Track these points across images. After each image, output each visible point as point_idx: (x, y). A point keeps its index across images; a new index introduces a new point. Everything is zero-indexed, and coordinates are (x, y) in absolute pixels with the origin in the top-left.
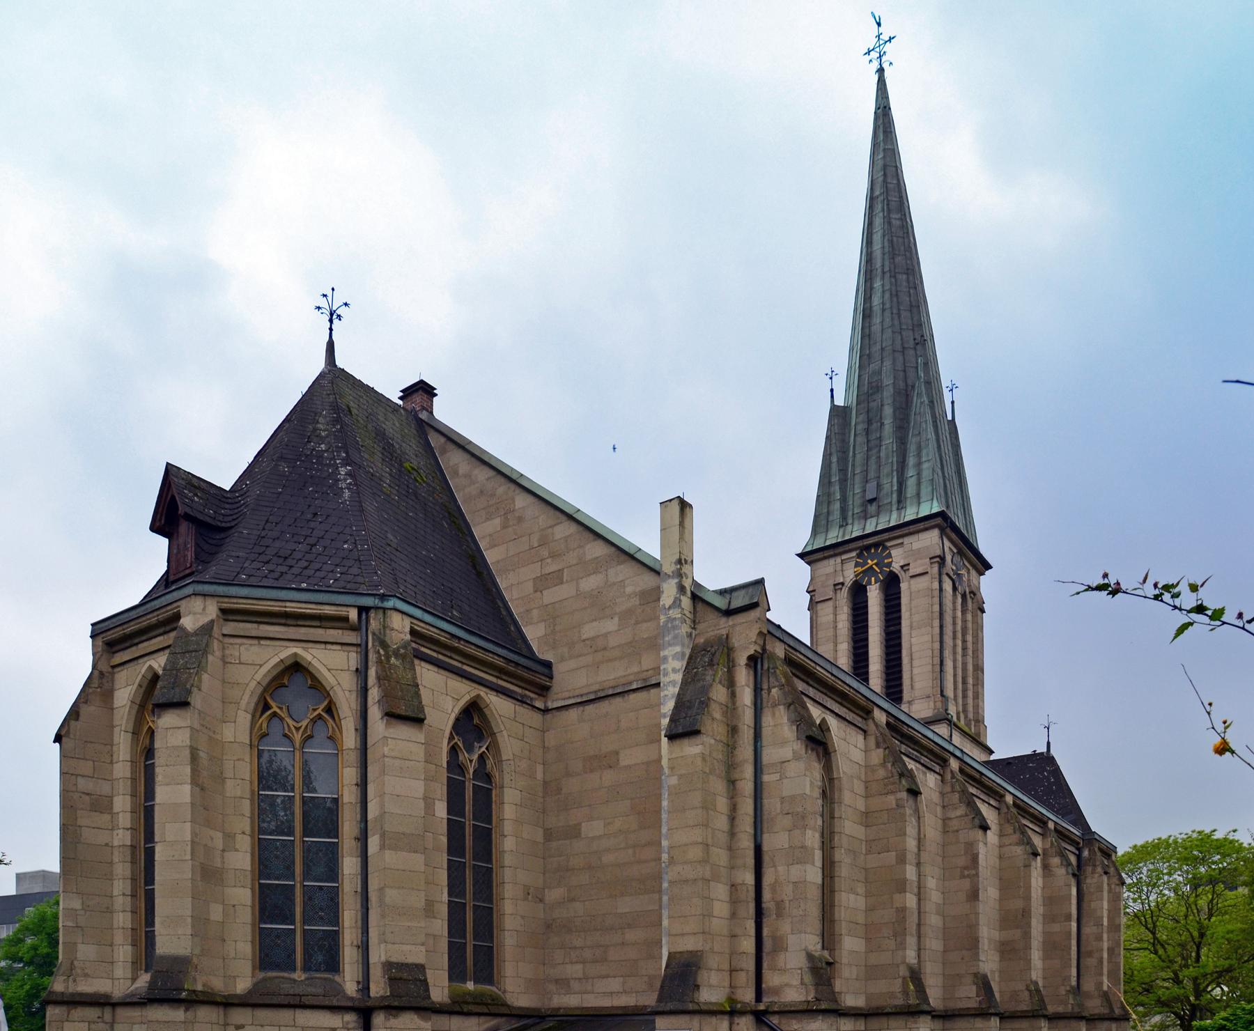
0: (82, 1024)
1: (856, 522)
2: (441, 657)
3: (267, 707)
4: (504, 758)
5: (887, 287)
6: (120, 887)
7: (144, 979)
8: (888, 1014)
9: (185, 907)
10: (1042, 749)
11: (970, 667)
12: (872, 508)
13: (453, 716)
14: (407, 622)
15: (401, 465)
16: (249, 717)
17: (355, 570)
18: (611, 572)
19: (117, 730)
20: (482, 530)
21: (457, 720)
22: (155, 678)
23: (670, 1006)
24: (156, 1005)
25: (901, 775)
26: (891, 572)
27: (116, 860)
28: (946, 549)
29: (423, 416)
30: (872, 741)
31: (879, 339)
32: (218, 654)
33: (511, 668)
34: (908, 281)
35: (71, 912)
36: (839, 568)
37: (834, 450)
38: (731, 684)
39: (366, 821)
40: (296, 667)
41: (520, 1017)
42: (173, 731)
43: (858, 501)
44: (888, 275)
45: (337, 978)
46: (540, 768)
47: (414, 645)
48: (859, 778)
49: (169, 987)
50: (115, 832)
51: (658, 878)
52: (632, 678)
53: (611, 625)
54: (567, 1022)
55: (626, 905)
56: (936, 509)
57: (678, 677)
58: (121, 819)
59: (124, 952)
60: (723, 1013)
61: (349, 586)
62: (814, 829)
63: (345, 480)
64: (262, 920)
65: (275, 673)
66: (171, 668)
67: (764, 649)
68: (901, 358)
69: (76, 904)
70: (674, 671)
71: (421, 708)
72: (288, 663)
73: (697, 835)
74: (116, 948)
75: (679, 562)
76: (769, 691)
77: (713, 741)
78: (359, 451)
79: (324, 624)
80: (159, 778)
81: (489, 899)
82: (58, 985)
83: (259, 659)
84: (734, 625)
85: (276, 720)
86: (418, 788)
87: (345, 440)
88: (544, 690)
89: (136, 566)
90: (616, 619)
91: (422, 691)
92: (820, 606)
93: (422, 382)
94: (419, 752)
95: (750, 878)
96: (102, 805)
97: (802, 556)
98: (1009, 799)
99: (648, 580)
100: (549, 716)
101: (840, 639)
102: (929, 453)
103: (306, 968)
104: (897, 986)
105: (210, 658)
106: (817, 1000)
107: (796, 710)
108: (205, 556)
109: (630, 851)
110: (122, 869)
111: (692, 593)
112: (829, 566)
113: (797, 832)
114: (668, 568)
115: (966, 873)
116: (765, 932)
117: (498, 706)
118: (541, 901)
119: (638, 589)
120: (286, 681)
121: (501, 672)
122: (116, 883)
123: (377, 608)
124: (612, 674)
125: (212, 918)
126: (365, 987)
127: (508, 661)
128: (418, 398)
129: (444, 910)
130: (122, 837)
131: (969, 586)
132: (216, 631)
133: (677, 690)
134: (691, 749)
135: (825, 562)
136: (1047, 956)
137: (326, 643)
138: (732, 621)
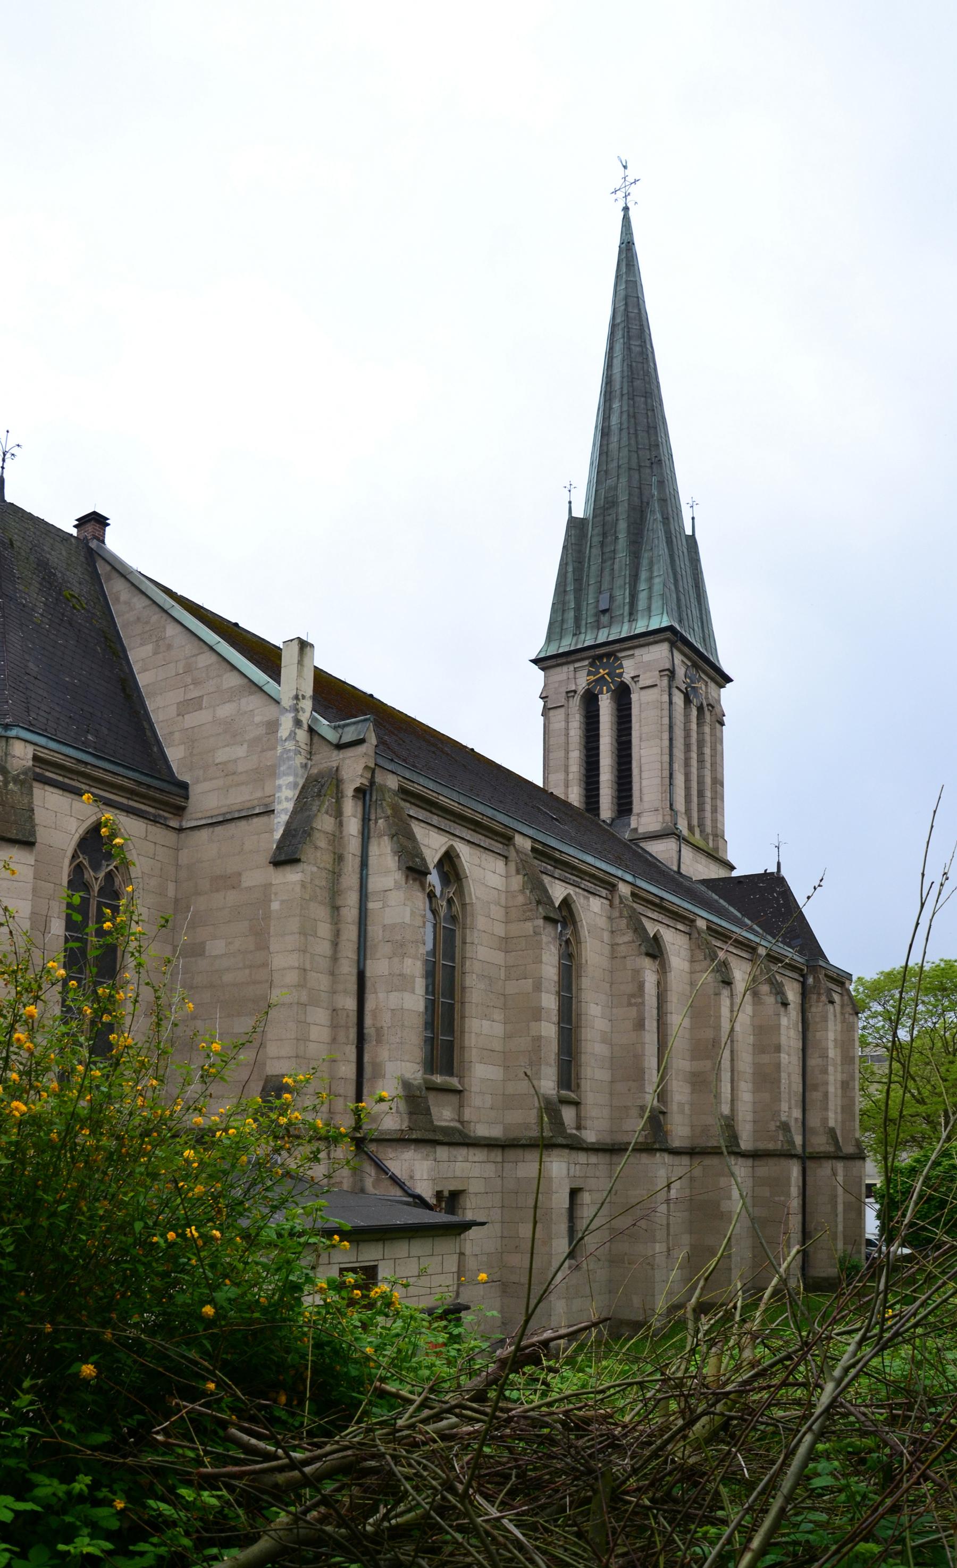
1: (589, 631)
5: (625, 409)
8: (524, 1146)
10: (772, 869)
11: (708, 780)
12: (605, 619)
13: (77, 837)
14: (30, 750)
15: (60, 593)
25: (539, 902)
26: (622, 682)
28: (676, 662)
29: (94, 544)
30: (512, 866)
31: (616, 457)
33: (143, 790)
34: (646, 403)
36: (572, 675)
37: (570, 560)
38: (338, 814)
43: (591, 610)
44: (625, 397)
46: (171, 887)
47: (38, 770)
48: (499, 904)
52: (256, 802)
53: (241, 751)
56: (664, 624)
57: (290, 806)
62: (415, 958)
67: (372, 782)
68: (637, 476)
70: (287, 799)
75: (296, 697)
76: (376, 822)
77: (315, 869)
84: (344, 759)
88: (179, 811)
90: (245, 746)
92: (552, 713)
93: (94, 513)
95: (351, 1003)
97: (535, 661)
98: (702, 924)
100: (183, 835)
101: (571, 747)
102: (661, 568)
104: (532, 1116)
106: (411, 1129)
107: (399, 842)
111: (309, 726)
112: (562, 674)
113: (396, 960)
115: (633, 1001)
116: (366, 1058)
119: (266, 719)
121: (131, 793)
127: (140, 783)
128: (90, 527)
131: (707, 698)
134: (292, 876)
135: (558, 669)
136: (757, 1089)
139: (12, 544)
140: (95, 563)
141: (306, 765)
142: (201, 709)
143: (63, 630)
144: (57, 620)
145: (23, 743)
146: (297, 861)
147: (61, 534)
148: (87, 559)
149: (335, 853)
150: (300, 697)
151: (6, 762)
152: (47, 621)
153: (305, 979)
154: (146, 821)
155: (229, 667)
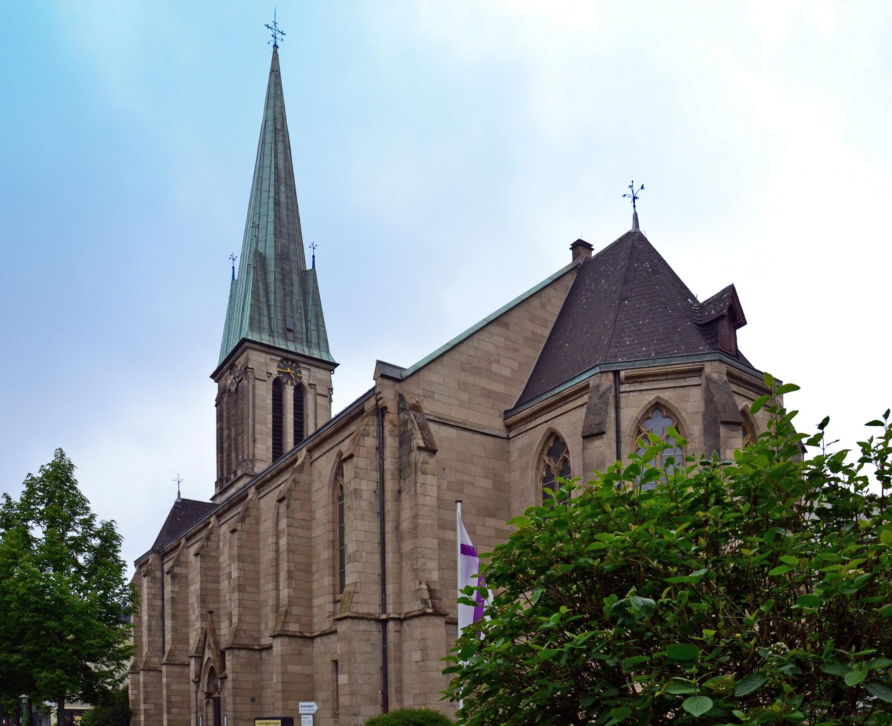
83: (634, 404)
93: (579, 240)
97: (336, 365)
135: (259, 353)
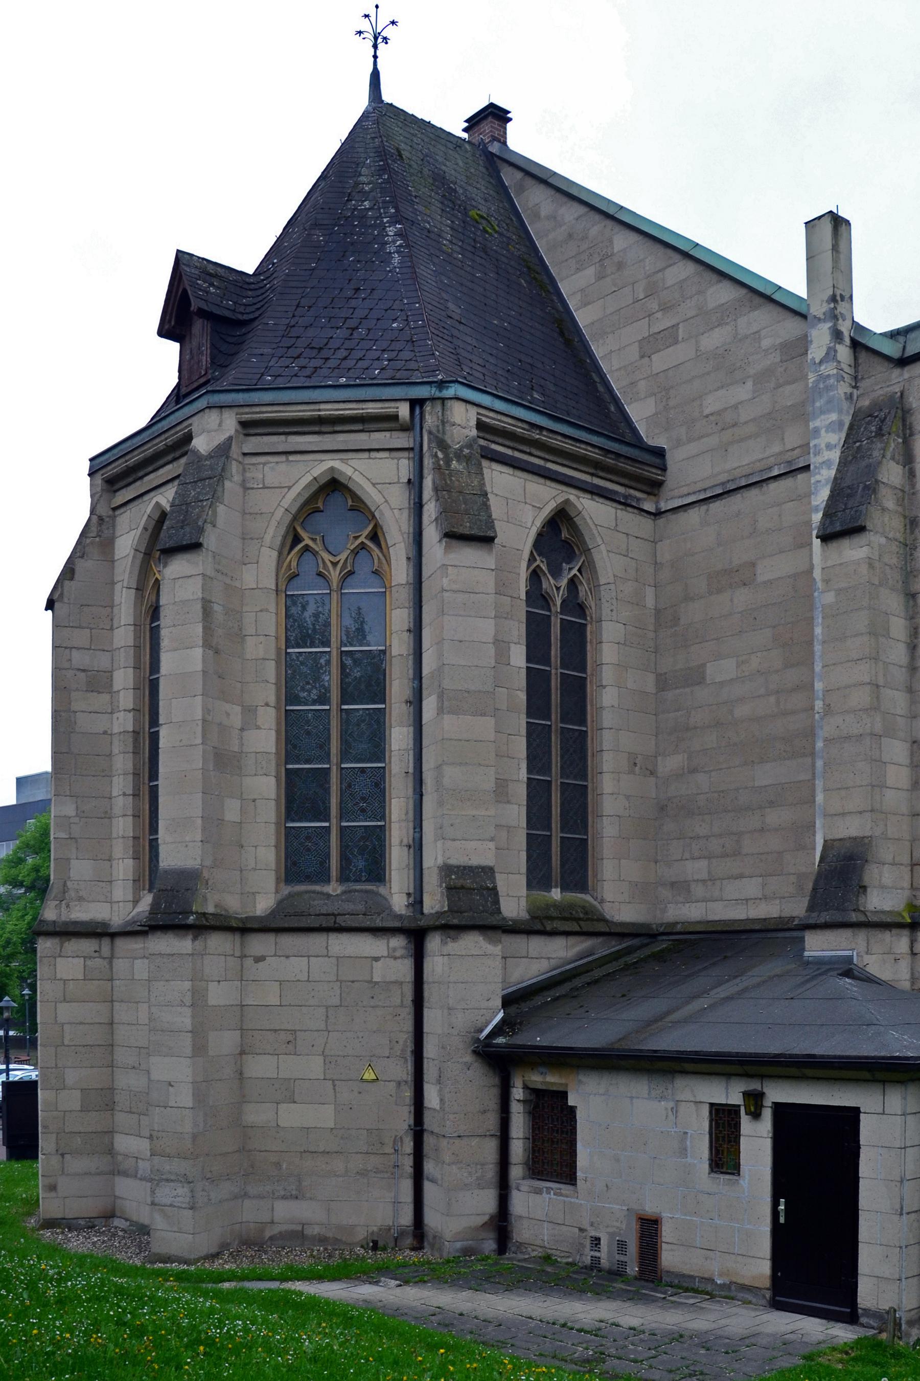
0: (76, 960)
2: (517, 454)
3: (297, 539)
4: (602, 581)
6: (120, 785)
7: (147, 900)
9: (195, 805)
14: (473, 412)
15: (466, 214)
16: (275, 554)
17: (406, 355)
18: (742, 321)
19: (118, 587)
20: (569, 287)
21: (540, 535)
22: (163, 515)
23: (825, 917)
24: (159, 933)
27: (116, 751)
29: (494, 148)
32: (237, 478)
33: (610, 461)
35: (64, 821)
39: (421, 678)
40: (333, 486)
41: (622, 935)
42: (181, 579)
45: (382, 890)
46: (650, 592)
47: (482, 442)
49: (175, 911)
50: (115, 716)
51: (810, 733)
52: (772, 460)
53: (743, 392)
54: (686, 941)
55: (767, 775)
57: (835, 456)
58: (121, 699)
59: (124, 868)
60: (901, 926)
61: (398, 375)
63: (394, 242)
64: (289, 817)
65: (306, 495)
66: (181, 503)
69: (69, 810)
70: (829, 447)
71: (490, 523)
72: (323, 481)
73: (862, 673)
74: (115, 863)
75: (833, 299)
77: (883, 540)
78: (412, 203)
79: (367, 426)
80: (165, 643)
81: (583, 774)
82: (50, 913)
83: (287, 478)
85: (308, 555)
86: (486, 628)
87: (394, 192)
88: (654, 487)
89: (144, 374)
90: (749, 384)
91: (493, 501)
93: (492, 106)
94: (488, 582)
96: (99, 682)
99: (790, 328)
100: (661, 521)
103: (344, 878)
105: (227, 484)
108: (222, 358)
109: (772, 699)
110: (123, 763)
114: (818, 309)
117: (594, 513)
118: (652, 773)
120: (320, 505)
121: (597, 467)
122: (115, 779)
123: (433, 399)
124: (745, 458)
125: (227, 818)
126: (417, 902)
127: (607, 452)
128: (487, 127)
129: (521, 792)
130: (123, 722)
132: (235, 451)
133: (833, 473)
134: (853, 551)
137: (370, 450)
138: (907, 372)
139: (400, 155)
140: (499, 172)
141: (851, 394)
142: (676, 342)
143: (478, 259)
144: (469, 248)
145: (464, 404)
146: (861, 529)
147: (452, 139)
148: (487, 169)
149: (905, 517)
150: (838, 298)
151: (444, 433)
152: (458, 249)
153: (878, 698)
154: (615, 505)
155: (714, 277)
